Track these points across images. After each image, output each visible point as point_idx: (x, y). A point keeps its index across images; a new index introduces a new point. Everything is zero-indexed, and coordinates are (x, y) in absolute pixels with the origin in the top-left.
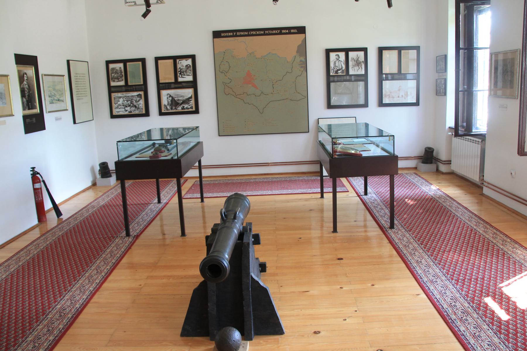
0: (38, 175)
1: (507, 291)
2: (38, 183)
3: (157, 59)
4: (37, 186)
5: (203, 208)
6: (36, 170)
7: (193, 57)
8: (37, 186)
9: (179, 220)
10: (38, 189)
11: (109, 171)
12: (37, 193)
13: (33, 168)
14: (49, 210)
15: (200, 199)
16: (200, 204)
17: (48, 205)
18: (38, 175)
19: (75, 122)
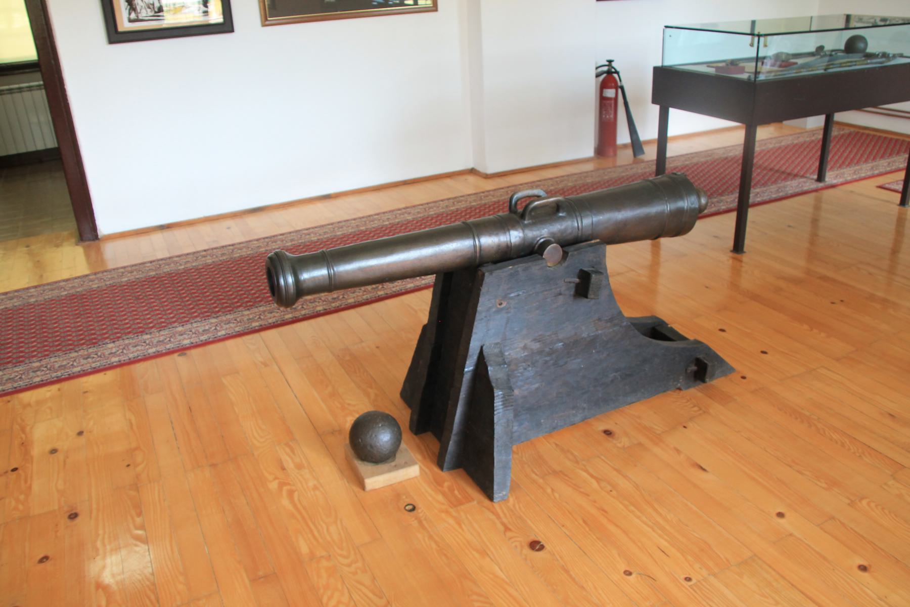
0: (615, 75)
1: (403, 445)
2: (611, 88)
3: (226, 26)
4: (610, 93)
5: (901, 221)
6: (613, 64)
7: (115, 36)
8: (610, 93)
9: (748, 229)
10: (610, 99)
11: (46, 89)
12: (603, 103)
13: (610, 62)
14: (625, 146)
15: (899, 196)
16: (896, 209)
17: (623, 137)
18: (615, 75)
19: (666, 27)
